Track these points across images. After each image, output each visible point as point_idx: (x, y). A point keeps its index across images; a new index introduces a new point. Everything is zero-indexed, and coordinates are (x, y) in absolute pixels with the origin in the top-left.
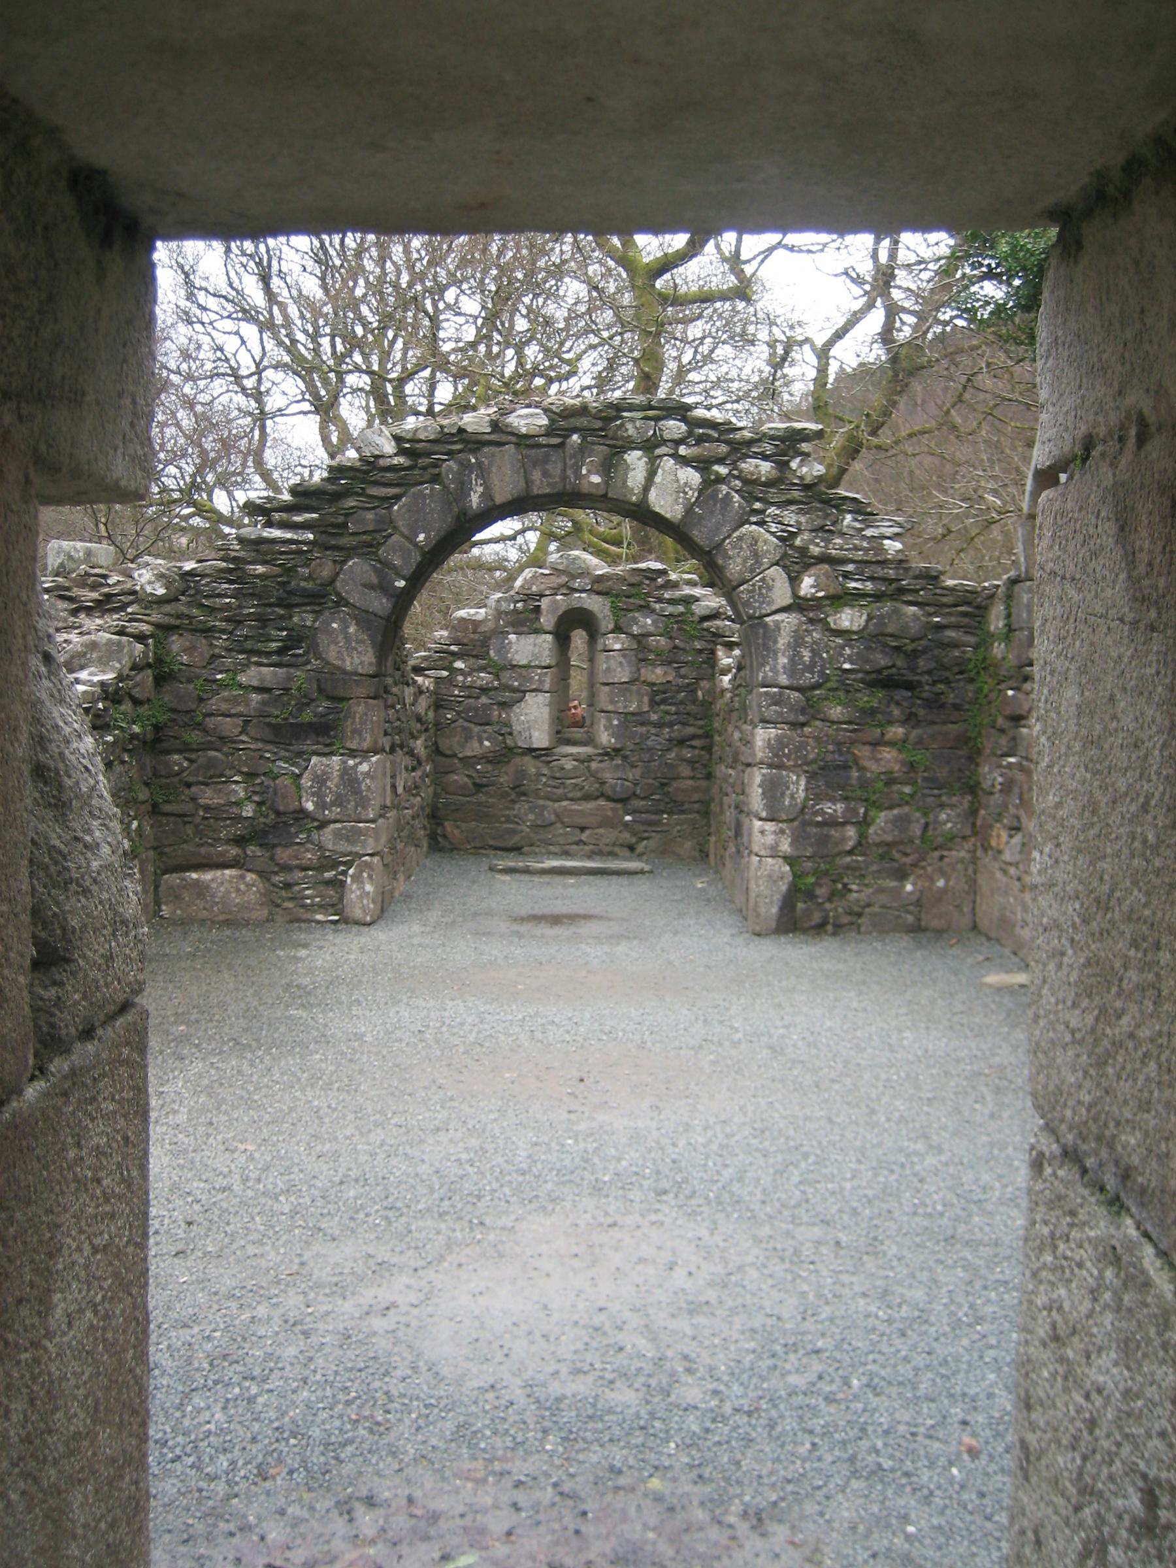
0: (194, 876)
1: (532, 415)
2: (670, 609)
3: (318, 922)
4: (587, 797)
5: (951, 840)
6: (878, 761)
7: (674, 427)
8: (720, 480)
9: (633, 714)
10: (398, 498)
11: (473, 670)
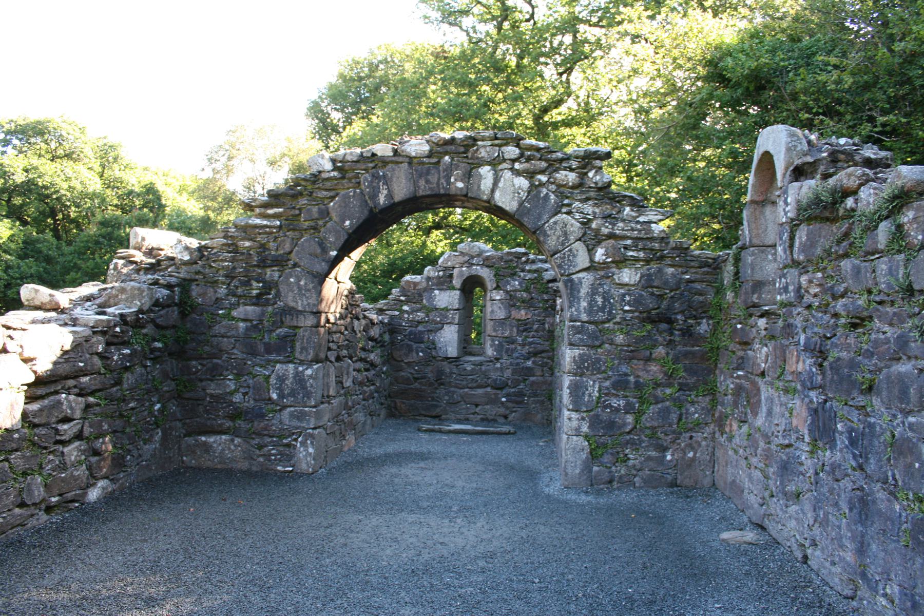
0: (203, 439)
4: (480, 387)
5: (699, 426)
6: (648, 371)
8: (542, 184)
9: (506, 337)
11: (413, 311)
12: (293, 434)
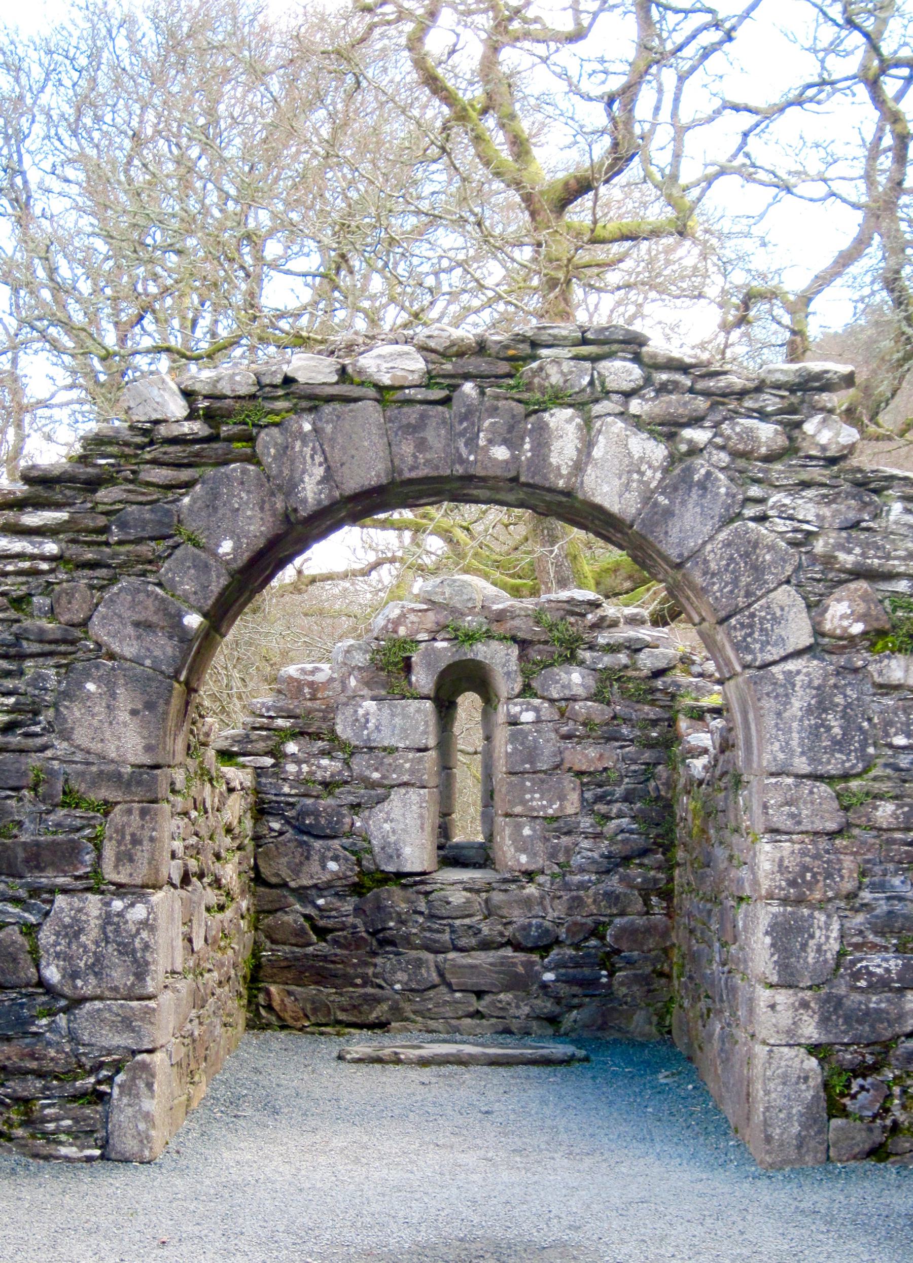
1: (400, 355)
2: (607, 660)
3: (68, 1159)
4: (486, 945)
7: (621, 372)
8: (695, 451)
10: (188, 485)
12: (101, 1065)
